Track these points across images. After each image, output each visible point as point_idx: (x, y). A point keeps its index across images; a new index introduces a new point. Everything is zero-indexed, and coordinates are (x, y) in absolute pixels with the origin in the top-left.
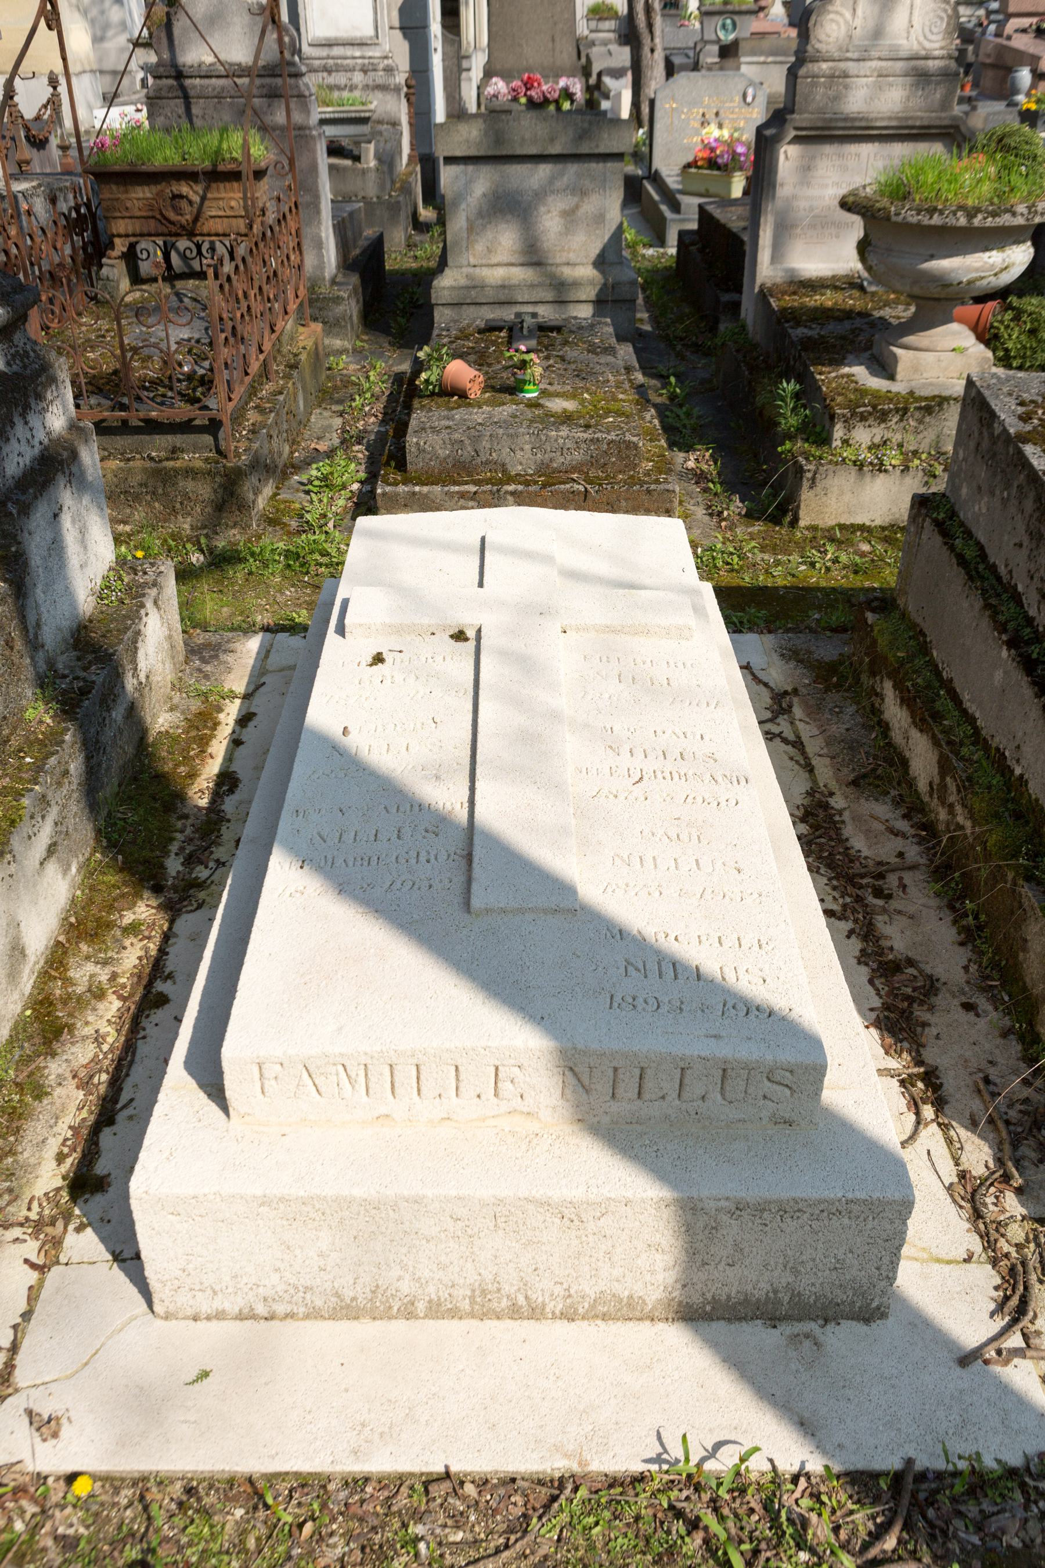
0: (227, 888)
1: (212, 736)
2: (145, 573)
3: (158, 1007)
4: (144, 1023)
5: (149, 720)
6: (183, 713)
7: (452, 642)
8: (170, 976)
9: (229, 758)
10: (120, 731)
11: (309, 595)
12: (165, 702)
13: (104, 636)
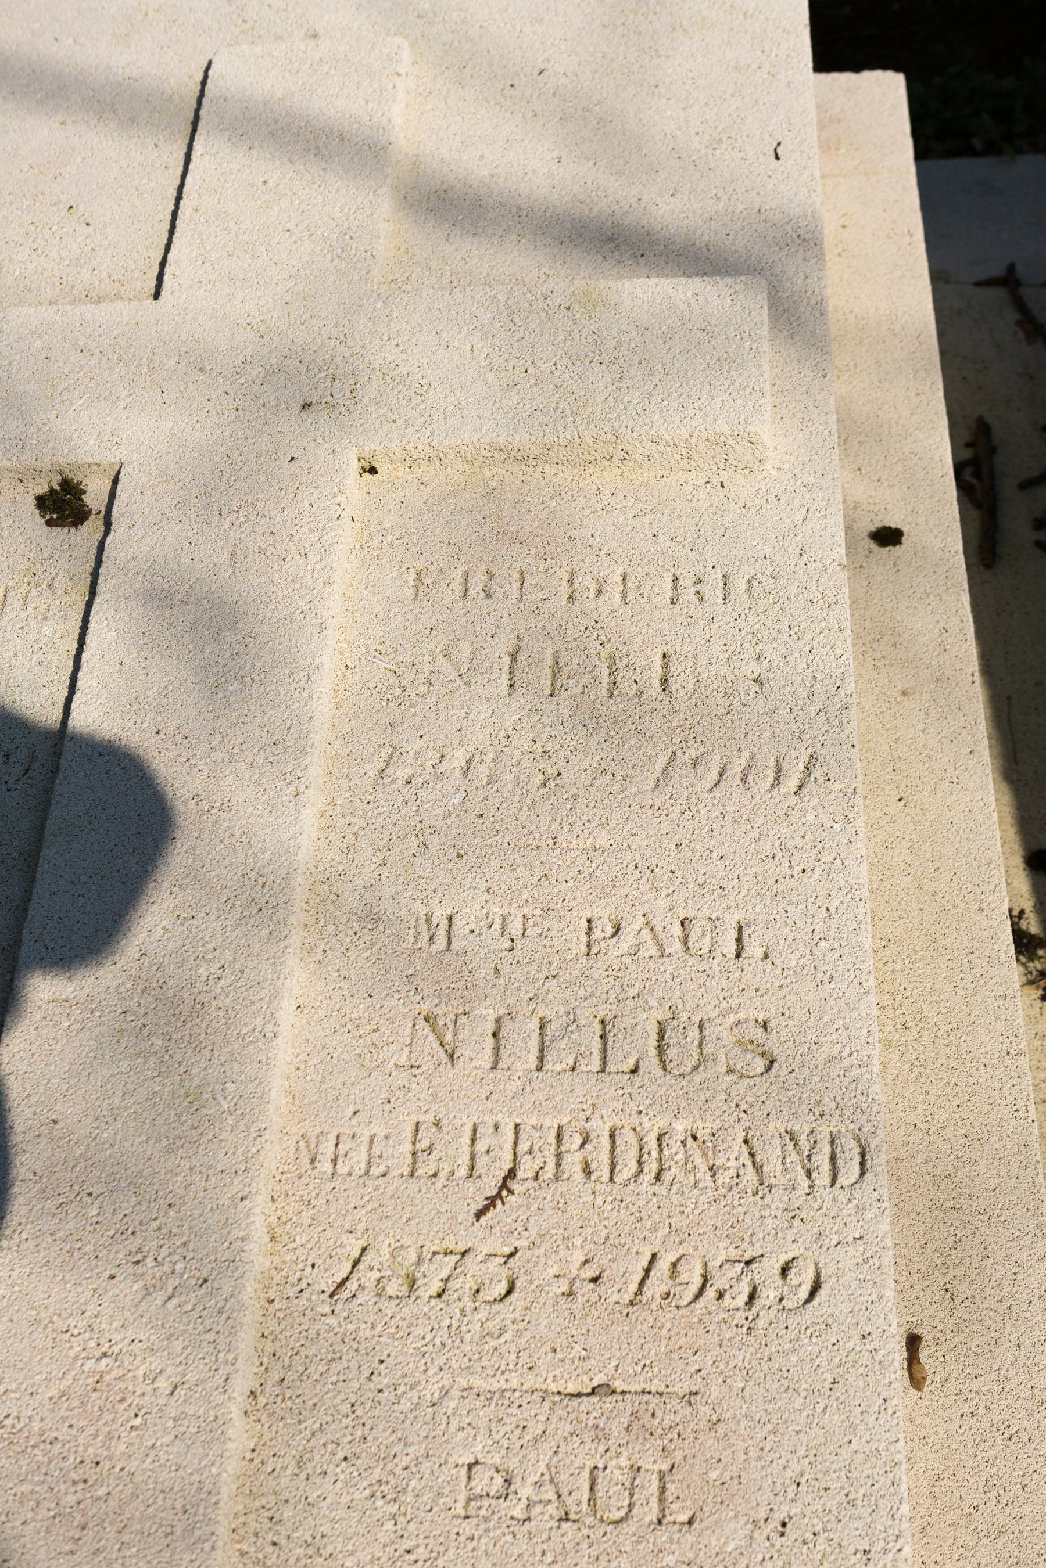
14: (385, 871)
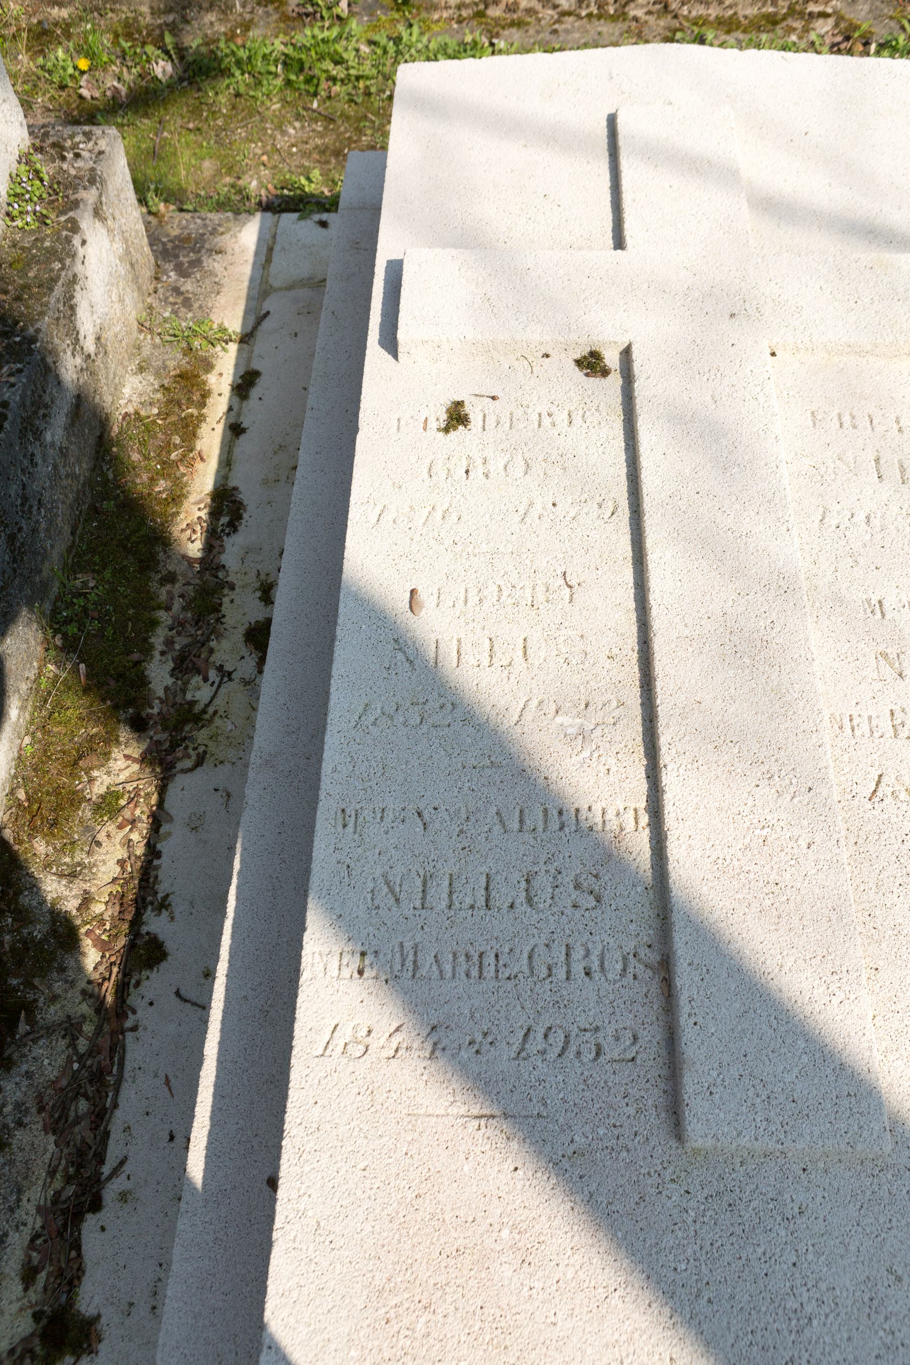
0: (235, 881)
1: (201, 418)
2: (77, 156)
3: (151, 967)
4: (133, 999)
5: (108, 399)
6: (157, 374)
7: (578, 375)
8: (163, 905)
9: (227, 462)
10: (63, 452)
11: (322, 136)
12: (132, 356)
13: (18, 298)
14: (838, 574)
